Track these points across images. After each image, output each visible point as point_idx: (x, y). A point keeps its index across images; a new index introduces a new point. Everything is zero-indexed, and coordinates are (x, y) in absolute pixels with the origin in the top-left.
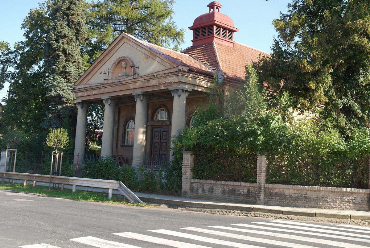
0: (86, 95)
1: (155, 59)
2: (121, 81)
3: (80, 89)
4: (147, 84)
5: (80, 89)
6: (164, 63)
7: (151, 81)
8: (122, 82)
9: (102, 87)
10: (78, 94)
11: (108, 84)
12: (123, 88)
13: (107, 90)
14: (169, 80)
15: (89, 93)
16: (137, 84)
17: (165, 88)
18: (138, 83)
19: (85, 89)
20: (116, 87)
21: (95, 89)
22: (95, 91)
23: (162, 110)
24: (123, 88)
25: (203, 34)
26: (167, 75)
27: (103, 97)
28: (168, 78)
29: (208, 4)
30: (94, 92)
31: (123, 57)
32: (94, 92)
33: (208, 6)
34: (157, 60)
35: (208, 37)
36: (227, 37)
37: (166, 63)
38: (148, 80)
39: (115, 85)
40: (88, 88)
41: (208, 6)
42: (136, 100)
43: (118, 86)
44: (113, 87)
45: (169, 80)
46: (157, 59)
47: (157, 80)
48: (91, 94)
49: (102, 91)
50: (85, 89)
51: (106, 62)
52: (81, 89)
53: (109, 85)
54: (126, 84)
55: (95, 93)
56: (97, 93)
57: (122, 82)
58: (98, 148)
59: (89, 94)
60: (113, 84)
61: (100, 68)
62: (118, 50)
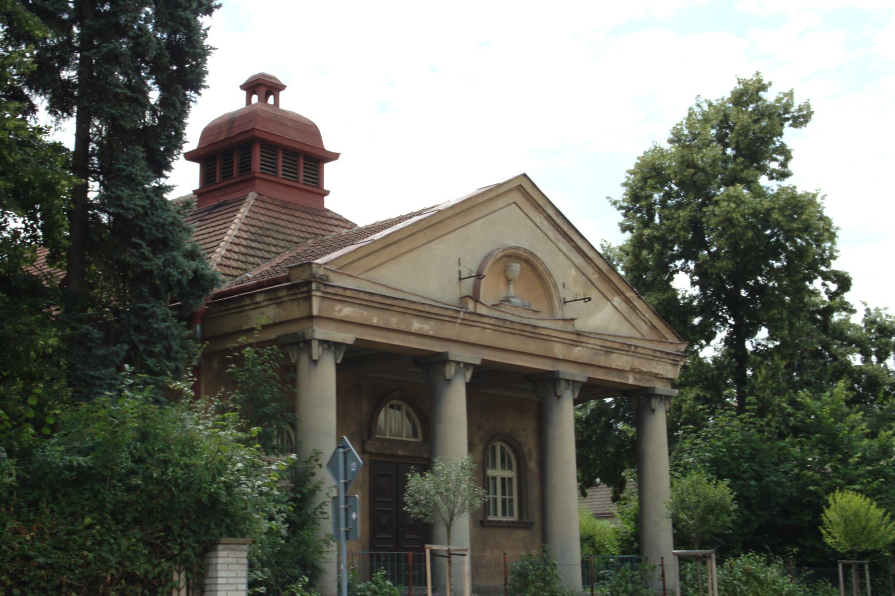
0: (375, 321)
1: (609, 297)
2: (535, 327)
3: (361, 296)
4: (602, 360)
5: (361, 296)
6: (634, 318)
7: (614, 355)
8: (538, 331)
9: (459, 321)
10: (338, 307)
11: (488, 317)
12: (531, 346)
13: (473, 334)
14: (656, 367)
15: (394, 321)
16: (577, 349)
17: (637, 383)
18: (579, 348)
19: (388, 302)
20: (509, 335)
21: (423, 315)
22: (422, 320)
23: (392, 407)
24: (531, 346)
25: (227, 173)
26: (658, 354)
27: (458, 354)
28: (655, 363)
29: (242, 82)
30: (416, 325)
31: (525, 250)
32: (416, 325)
33: (243, 87)
34: (614, 303)
35: (222, 184)
36: (302, 178)
37: (639, 321)
38: (608, 351)
39: (400, 310)
40: (403, 304)
41: (243, 87)
42: (293, 361)
43: (515, 336)
44: (497, 333)
45: (656, 367)
46: (617, 300)
47: (629, 358)
48: (403, 327)
49: (451, 331)
50: (388, 302)
51: (448, 233)
52: (367, 297)
53: (492, 322)
54: (547, 339)
55: (421, 329)
56: (431, 333)
57: (538, 331)
58: (126, 499)
59: (394, 326)
60: (508, 324)
61: (423, 245)
62: (492, 216)
